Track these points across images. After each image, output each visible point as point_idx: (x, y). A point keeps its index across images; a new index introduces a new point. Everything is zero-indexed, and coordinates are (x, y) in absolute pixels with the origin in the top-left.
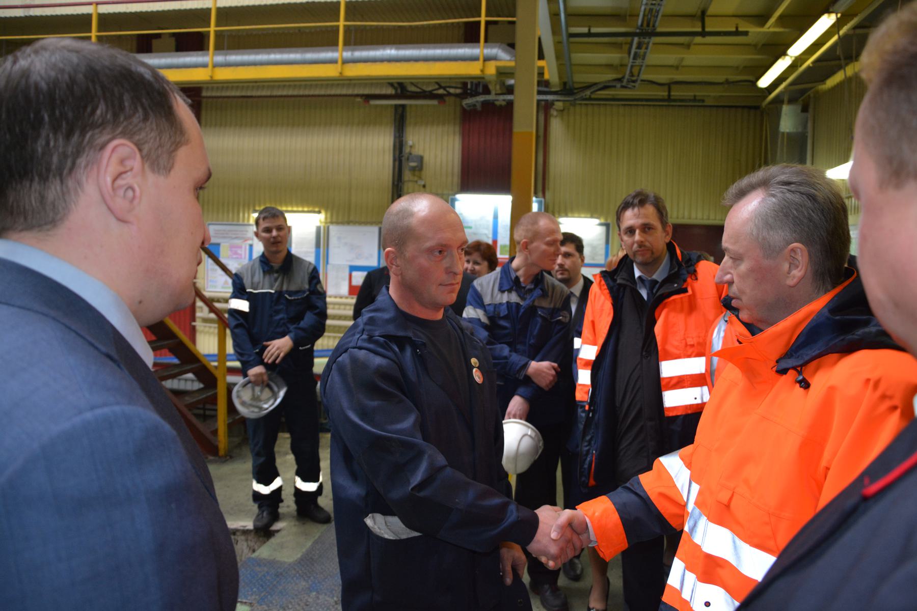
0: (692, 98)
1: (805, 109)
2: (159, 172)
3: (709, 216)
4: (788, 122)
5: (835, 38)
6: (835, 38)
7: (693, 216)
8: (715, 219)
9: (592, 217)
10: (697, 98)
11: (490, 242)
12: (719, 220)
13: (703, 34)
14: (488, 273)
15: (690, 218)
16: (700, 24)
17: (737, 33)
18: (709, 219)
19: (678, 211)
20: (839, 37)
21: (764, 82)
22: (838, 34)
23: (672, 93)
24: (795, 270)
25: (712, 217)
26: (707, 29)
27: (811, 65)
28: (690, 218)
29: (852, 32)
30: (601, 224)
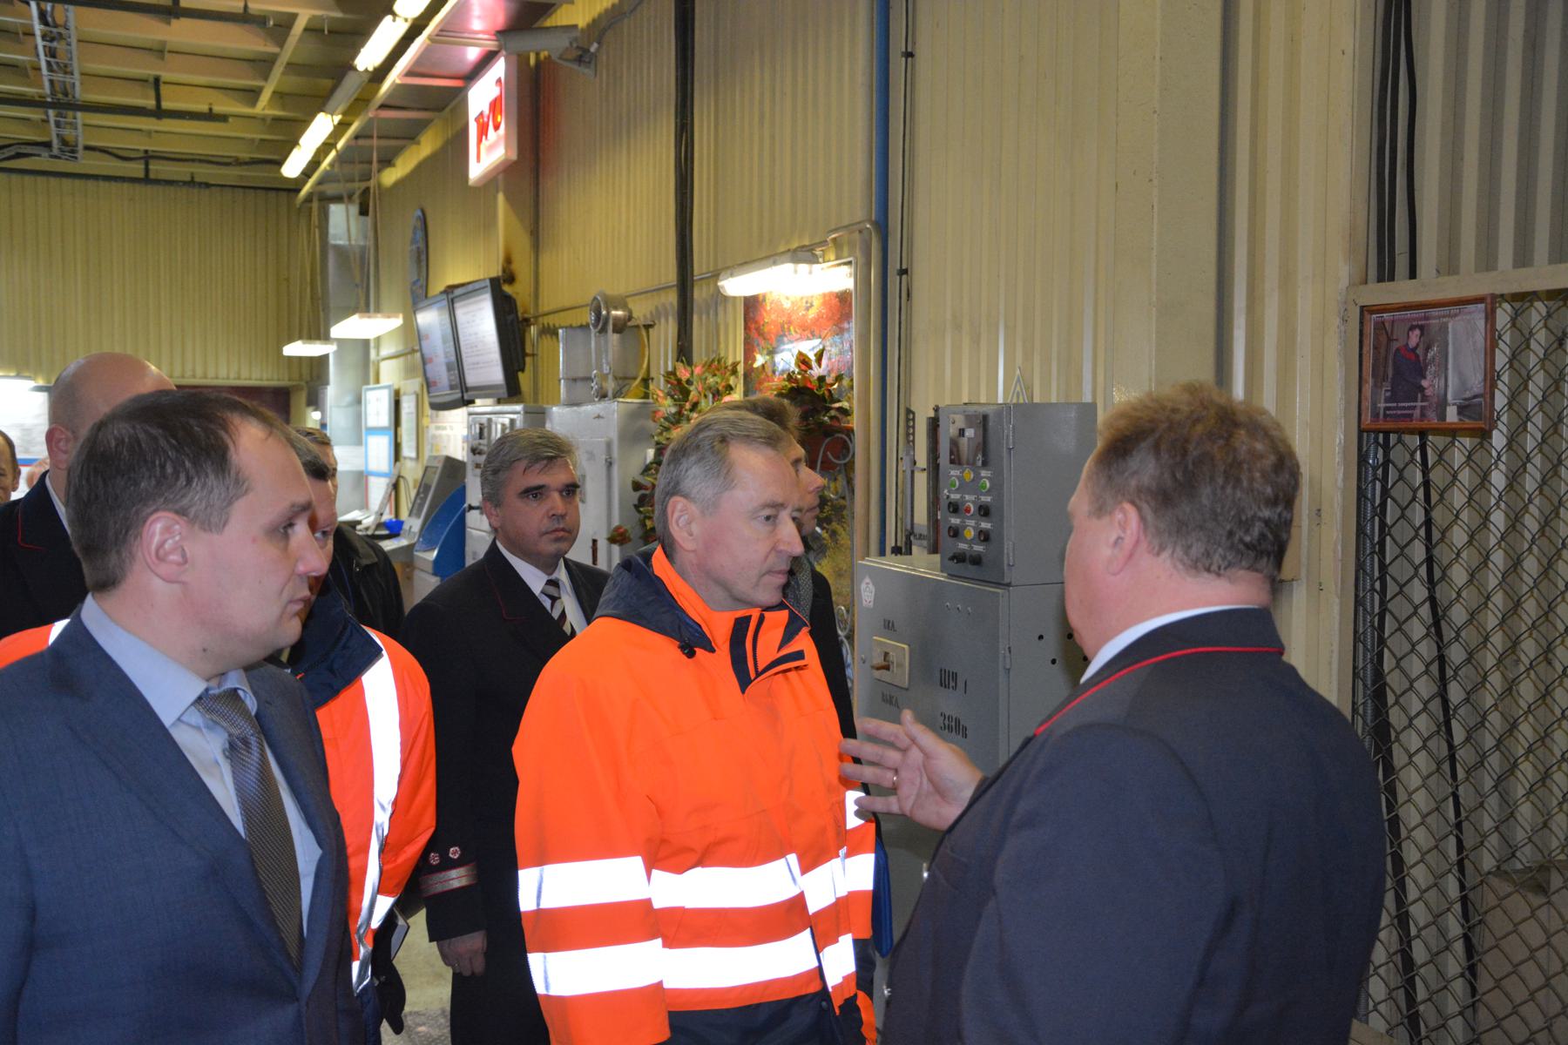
0: (188, 178)
1: (364, 211)
2: (211, 530)
3: (239, 373)
4: (342, 222)
5: (333, 154)
6: (333, 154)
7: (211, 373)
8: (250, 379)
9: (19, 376)
10: (197, 179)
11: (655, 872)
12: (235, 379)
13: (159, 113)
14: (305, 464)
15: (205, 377)
16: (152, 93)
17: (210, 116)
18: (239, 378)
19: (183, 364)
20: (336, 148)
21: (293, 167)
22: (337, 151)
23: (143, 167)
24: (332, 450)
25: (245, 374)
26: (166, 105)
27: (328, 168)
28: (205, 377)
29: (353, 143)
30: (39, 389)
